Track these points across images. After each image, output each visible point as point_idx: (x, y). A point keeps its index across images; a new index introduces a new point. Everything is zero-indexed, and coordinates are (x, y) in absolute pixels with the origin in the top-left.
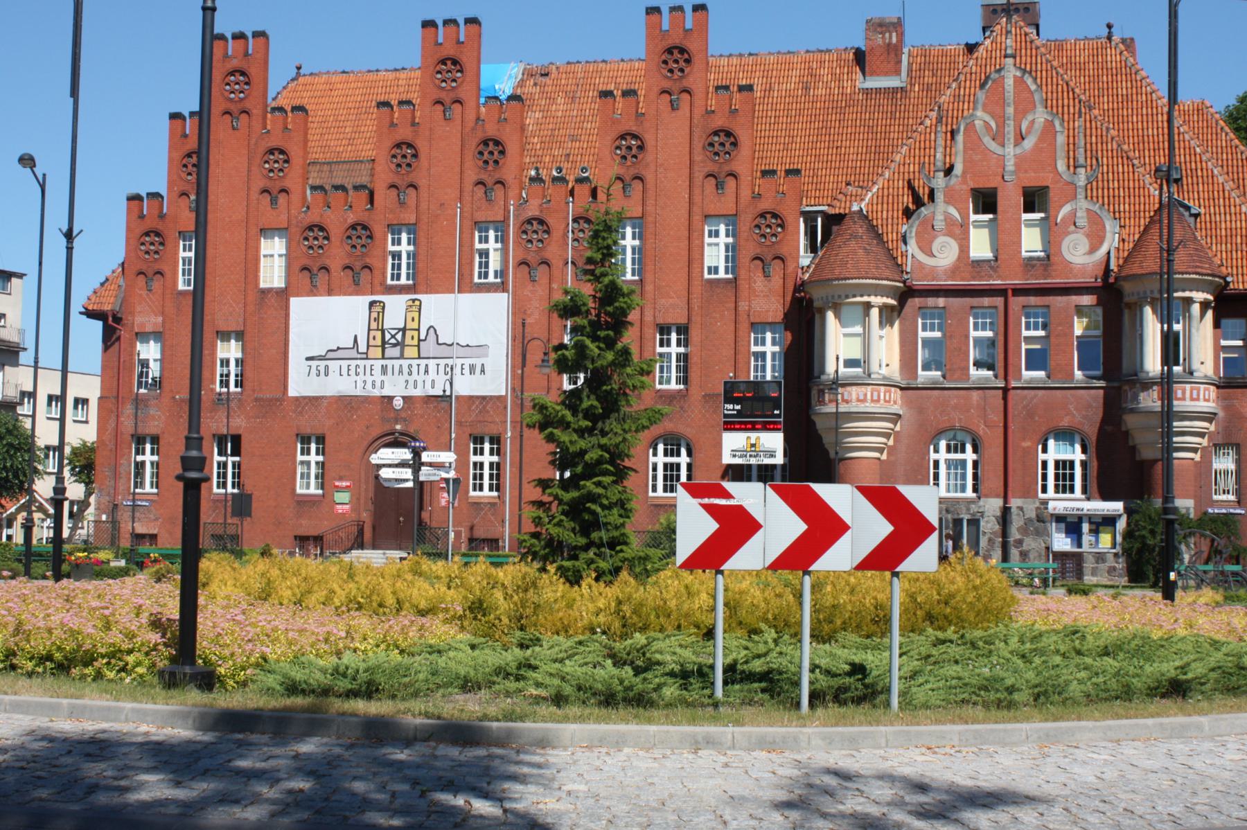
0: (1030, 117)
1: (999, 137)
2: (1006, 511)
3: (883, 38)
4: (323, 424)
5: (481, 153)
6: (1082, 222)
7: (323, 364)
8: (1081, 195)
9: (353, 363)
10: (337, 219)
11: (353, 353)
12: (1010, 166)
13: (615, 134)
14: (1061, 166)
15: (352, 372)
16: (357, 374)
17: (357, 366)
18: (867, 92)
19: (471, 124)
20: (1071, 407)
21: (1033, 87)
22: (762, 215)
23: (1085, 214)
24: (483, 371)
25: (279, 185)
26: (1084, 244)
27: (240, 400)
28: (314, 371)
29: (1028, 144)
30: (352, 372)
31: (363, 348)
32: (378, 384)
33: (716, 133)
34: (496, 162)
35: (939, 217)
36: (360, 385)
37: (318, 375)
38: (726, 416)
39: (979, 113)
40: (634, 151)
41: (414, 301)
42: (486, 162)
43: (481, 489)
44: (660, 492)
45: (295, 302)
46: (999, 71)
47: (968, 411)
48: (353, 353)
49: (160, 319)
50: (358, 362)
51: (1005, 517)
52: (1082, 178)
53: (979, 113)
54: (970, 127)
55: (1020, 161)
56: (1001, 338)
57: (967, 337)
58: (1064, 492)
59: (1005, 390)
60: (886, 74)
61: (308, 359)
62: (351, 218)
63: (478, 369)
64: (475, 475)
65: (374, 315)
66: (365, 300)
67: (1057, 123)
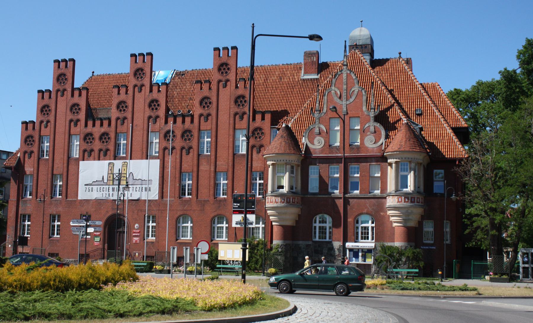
3: (311, 59)
4: (91, 210)
7: (91, 187)
9: (102, 187)
11: (102, 183)
15: (102, 190)
16: (103, 191)
17: (136, 188)
18: (304, 80)
20: (368, 205)
21: (354, 77)
24: (150, 190)
28: (87, 190)
30: (102, 190)
31: (105, 181)
32: (111, 195)
36: (104, 195)
37: (89, 191)
38: (234, 208)
39: (333, 88)
41: (125, 162)
45: (81, 163)
48: (102, 183)
49: (32, 169)
50: (104, 186)
53: (333, 88)
56: (36, 172)
58: (365, 239)
61: (85, 185)
63: (148, 189)
65: (110, 168)
66: (107, 162)
67: (363, 91)
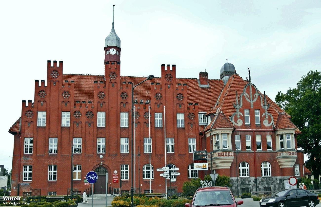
0: (255, 95)
1: (249, 98)
2: (256, 179)
5: (122, 95)
6: (267, 117)
8: (266, 112)
10: (84, 109)
12: (252, 105)
13: (155, 93)
14: (262, 105)
18: (202, 88)
19: (119, 88)
22: (190, 113)
23: (267, 116)
25: (67, 101)
26: (268, 122)
27: (56, 156)
29: (255, 100)
33: (179, 94)
34: (126, 98)
35: (238, 115)
39: (245, 93)
40: (160, 97)
42: (123, 98)
43: (51, 179)
44: (145, 178)
46: (249, 84)
47: (246, 158)
51: (255, 181)
52: (266, 108)
54: (243, 96)
55: (254, 103)
57: (97, 145)
59: (255, 153)
60: (205, 84)
62: (88, 110)
64: (31, 177)
